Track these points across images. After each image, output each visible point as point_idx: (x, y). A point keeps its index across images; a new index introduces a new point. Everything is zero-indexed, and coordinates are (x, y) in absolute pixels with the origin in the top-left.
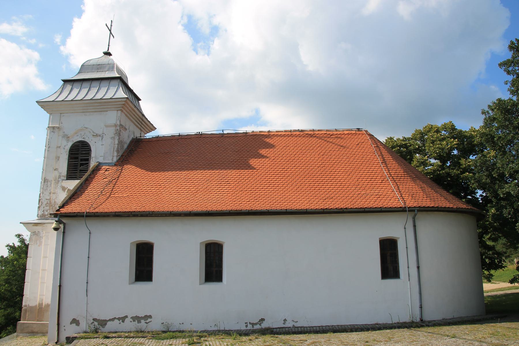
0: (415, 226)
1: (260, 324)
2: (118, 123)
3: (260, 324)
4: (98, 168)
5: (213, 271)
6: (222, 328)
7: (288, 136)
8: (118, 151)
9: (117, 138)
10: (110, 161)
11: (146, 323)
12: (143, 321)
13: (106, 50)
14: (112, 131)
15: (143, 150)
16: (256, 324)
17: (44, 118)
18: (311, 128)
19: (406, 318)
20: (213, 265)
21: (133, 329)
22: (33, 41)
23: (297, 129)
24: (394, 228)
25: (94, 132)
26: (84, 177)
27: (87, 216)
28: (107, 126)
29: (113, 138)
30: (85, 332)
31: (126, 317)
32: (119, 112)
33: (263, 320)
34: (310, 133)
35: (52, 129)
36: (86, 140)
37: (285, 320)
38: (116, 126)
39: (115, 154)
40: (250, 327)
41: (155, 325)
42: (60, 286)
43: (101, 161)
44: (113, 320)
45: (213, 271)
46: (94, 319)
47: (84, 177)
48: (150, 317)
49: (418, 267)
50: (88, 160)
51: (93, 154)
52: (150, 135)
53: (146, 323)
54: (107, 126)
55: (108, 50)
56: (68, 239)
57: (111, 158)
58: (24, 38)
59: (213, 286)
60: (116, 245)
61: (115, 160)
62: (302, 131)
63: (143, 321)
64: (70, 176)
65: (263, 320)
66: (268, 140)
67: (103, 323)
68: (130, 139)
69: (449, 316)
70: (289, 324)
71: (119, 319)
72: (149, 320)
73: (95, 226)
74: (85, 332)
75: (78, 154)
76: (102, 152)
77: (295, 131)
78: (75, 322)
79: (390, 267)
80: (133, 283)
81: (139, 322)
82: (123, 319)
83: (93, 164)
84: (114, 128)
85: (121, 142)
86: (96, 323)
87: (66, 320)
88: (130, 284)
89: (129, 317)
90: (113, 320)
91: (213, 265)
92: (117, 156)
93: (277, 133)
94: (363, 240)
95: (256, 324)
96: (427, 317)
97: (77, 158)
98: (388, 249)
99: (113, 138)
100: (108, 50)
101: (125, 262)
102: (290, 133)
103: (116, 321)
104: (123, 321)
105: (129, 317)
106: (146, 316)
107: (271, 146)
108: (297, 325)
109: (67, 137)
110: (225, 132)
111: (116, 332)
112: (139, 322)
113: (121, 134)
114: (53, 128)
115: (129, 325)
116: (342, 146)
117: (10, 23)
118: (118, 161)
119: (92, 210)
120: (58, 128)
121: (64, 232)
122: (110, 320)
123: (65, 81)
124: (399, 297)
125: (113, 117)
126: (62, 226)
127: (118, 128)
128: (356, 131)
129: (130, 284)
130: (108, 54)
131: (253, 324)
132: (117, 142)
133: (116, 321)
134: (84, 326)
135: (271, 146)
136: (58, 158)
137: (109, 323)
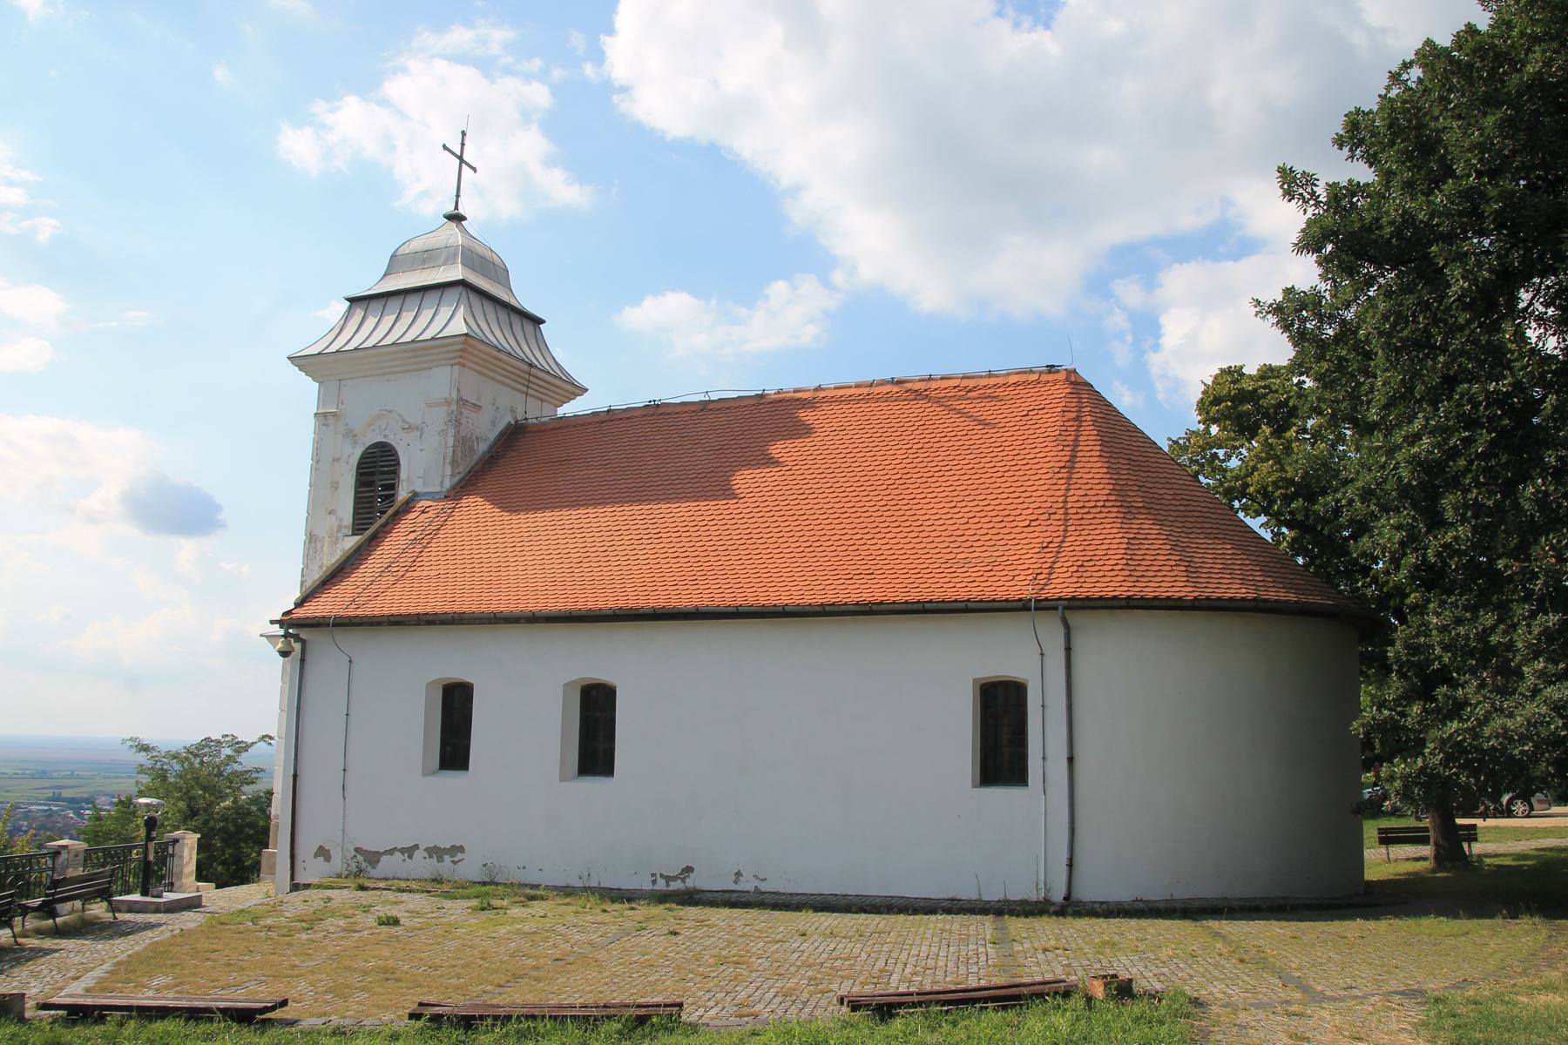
0: (1068, 649)
1: (683, 881)
2: (454, 396)
3: (683, 881)
4: (408, 506)
5: (595, 751)
6: (594, 884)
7: (859, 399)
8: (454, 463)
9: (451, 432)
10: (437, 489)
11: (455, 863)
12: (447, 858)
13: (450, 209)
14: (438, 418)
15: (534, 451)
16: (674, 878)
17: (307, 390)
18: (925, 373)
19: (1023, 889)
20: (595, 737)
21: (427, 876)
22: (537, 64)
23: (888, 377)
24: (1014, 653)
25: (404, 421)
26: (368, 533)
27: (336, 625)
28: (430, 405)
29: (443, 433)
30: (339, 876)
31: (416, 847)
32: (456, 368)
33: (689, 869)
34: (917, 386)
35: (322, 417)
36: (391, 440)
37: (738, 874)
38: (448, 403)
39: (448, 470)
40: (661, 885)
41: (470, 868)
42: (295, 776)
43: (419, 490)
44: (391, 852)
45: (595, 751)
46: (357, 850)
47: (368, 533)
48: (461, 849)
49: (1071, 760)
50: (392, 487)
51: (403, 474)
52: (568, 409)
53: (455, 863)
54: (430, 405)
55: (456, 208)
56: (1079, 643)
57: (437, 482)
58: (510, 60)
59: (453, 779)
60: (402, 685)
61: (447, 484)
62: (900, 382)
63: (447, 858)
64: (356, 531)
65: (689, 869)
66: (802, 414)
67: (373, 858)
68: (501, 426)
69: (1182, 893)
70: (747, 885)
71: (403, 851)
72: (459, 856)
73: (353, 642)
74: (339, 876)
75: (372, 474)
76: (422, 468)
77: (883, 383)
78: (323, 853)
79: (1001, 750)
80: (433, 773)
81: (440, 859)
82: (410, 851)
83: (402, 494)
84: (444, 408)
85: (463, 443)
86: (360, 858)
87: (306, 848)
88: (424, 775)
89: (422, 847)
90: (391, 852)
91: (595, 737)
92: (452, 476)
93: (841, 392)
94: (937, 680)
95: (674, 878)
96: (1087, 891)
97: (371, 484)
98: (456, 705)
99: (443, 433)
100: (456, 208)
101: (417, 725)
102: (866, 391)
103: (397, 854)
104: (410, 857)
105: (422, 847)
106: (453, 847)
107: (805, 430)
108: (764, 887)
109: (351, 435)
110: (714, 397)
111: (387, 879)
112: (440, 859)
113: (463, 421)
114: (325, 415)
115: (422, 866)
116: (981, 422)
117: (469, 24)
118: (453, 488)
119: (351, 612)
120: (334, 414)
121: (303, 660)
122: (386, 853)
123: (353, 301)
124: (1013, 835)
125: (442, 381)
126: (297, 646)
127: (454, 407)
128: (1041, 373)
129: (424, 775)
130: (456, 218)
131: (668, 879)
132: (451, 442)
133: (397, 854)
134: (337, 863)
135: (805, 430)
136: (335, 486)
137: (384, 859)
